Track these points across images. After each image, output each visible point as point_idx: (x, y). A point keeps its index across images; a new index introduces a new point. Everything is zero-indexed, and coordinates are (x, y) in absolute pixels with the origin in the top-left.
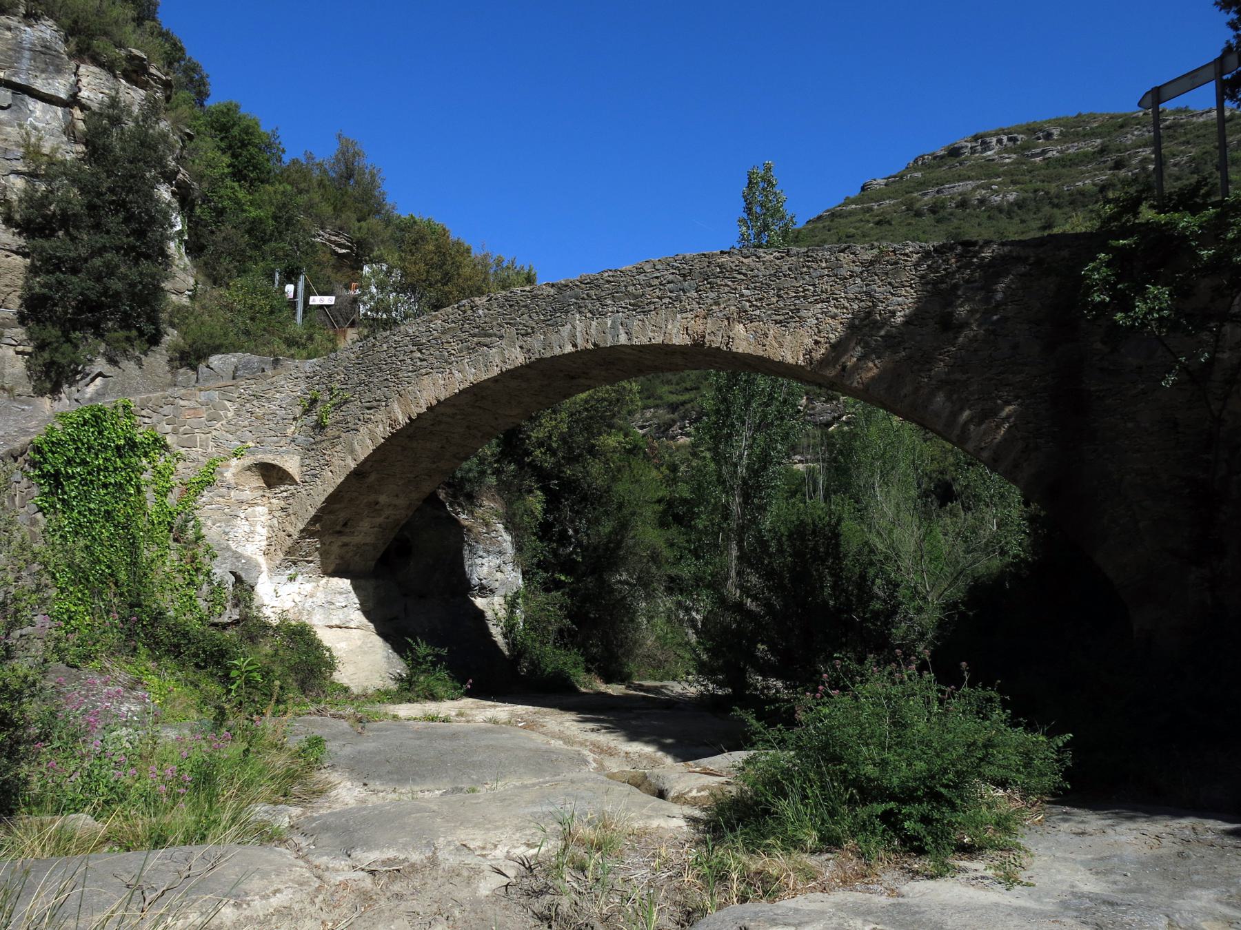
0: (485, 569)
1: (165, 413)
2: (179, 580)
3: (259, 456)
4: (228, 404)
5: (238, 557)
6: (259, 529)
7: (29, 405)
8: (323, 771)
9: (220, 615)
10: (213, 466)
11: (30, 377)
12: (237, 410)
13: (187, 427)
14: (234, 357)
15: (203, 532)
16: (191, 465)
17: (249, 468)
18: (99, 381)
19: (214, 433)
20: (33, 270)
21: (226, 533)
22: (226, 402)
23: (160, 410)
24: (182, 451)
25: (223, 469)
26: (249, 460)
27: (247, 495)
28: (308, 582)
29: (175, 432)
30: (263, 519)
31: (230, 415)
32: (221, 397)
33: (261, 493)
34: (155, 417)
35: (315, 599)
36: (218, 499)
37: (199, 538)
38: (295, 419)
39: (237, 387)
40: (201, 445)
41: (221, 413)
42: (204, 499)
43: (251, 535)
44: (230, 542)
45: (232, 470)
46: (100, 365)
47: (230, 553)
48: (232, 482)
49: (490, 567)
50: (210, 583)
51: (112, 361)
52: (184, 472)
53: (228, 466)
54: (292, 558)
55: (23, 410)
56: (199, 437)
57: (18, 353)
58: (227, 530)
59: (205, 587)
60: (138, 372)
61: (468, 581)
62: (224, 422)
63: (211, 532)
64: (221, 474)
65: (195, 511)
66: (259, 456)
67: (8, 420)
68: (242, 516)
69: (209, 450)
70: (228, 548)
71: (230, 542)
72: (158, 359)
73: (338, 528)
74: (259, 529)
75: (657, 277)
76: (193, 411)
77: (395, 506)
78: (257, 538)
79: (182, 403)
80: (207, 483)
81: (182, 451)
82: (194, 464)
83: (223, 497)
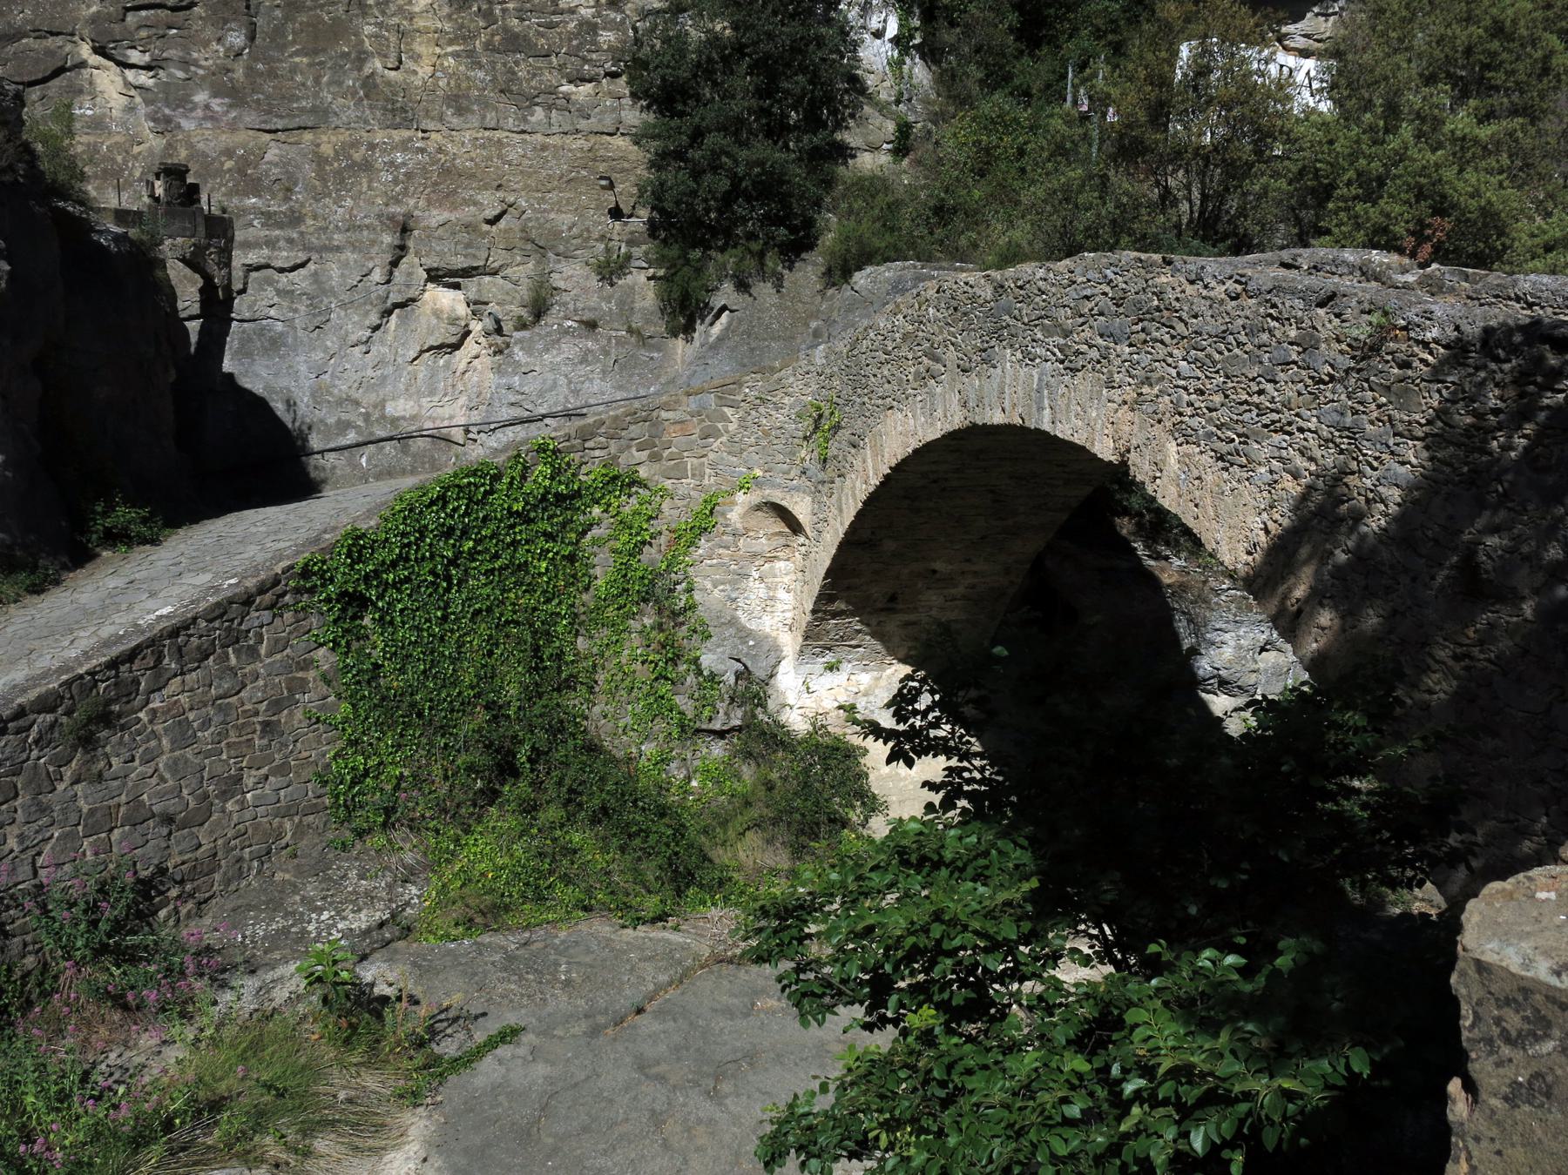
0: (1228, 652)
1: (632, 435)
2: (643, 673)
3: (767, 492)
4: (728, 411)
5: (744, 634)
6: (781, 594)
7: (659, 350)
8: (421, 1109)
9: (710, 719)
10: (712, 508)
11: (662, 311)
12: (742, 419)
13: (673, 449)
14: (889, 269)
15: (697, 596)
16: (680, 503)
17: (758, 508)
18: (725, 316)
19: (711, 456)
20: (658, 163)
21: (734, 600)
22: (726, 409)
23: (624, 433)
24: (668, 484)
25: (726, 508)
26: (755, 497)
27: (763, 544)
28: (864, 671)
29: (655, 458)
30: (786, 579)
31: (732, 427)
32: (719, 403)
33: (782, 541)
34: (613, 447)
35: (871, 698)
36: (721, 551)
37: (692, 607)
38: (805, 438)
39: (741, 385)
40: (693, 475)
41: (720, 426)
42: (700, 551)
43: (768, 602)
44: (739, 613)
45: (737, 511)
46: (726, 294)
47: (732, 631)
48: (739, 526)
49: (1240, 647)
50: (699, 672)
51: (742, 286)
52: (672, 514)
53: (734, 503)
54: (816, 639)
55: (652, 358)
56: (691, 463)
57: (649, 279)
58: (734, 596)
59: (691, 679)
60: (775, 299)
61: (1194, 675)
62: (724, 439)
63: (709, 594)
64: (723, 514)
65: (689, 569)
66: (767, 492)
67: (631, 376)
68: (756, 575)
69: (706, 482)
70: (733, 622)
71: (739, 613)
72: (807, 274)
73: (879, 605)
74: (781, 594)
75: (1087, 298)
76: (678, 427)
77: (975, 572)
78: (779, 607)
79: (664, 415)
80: (701, 529)
81: (668, 484)
82: (685, 502)
83: (727, 548)
